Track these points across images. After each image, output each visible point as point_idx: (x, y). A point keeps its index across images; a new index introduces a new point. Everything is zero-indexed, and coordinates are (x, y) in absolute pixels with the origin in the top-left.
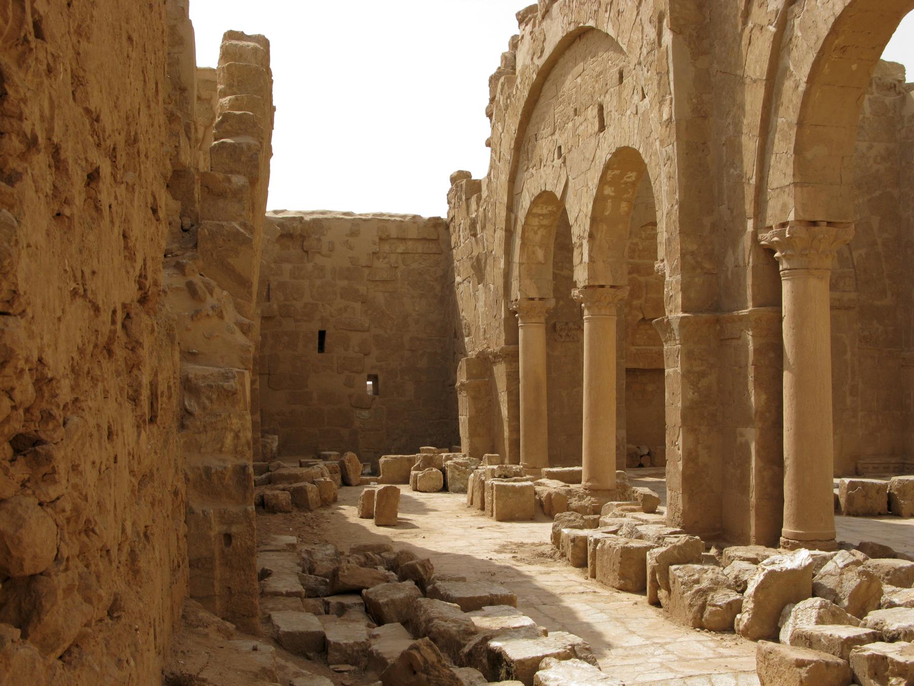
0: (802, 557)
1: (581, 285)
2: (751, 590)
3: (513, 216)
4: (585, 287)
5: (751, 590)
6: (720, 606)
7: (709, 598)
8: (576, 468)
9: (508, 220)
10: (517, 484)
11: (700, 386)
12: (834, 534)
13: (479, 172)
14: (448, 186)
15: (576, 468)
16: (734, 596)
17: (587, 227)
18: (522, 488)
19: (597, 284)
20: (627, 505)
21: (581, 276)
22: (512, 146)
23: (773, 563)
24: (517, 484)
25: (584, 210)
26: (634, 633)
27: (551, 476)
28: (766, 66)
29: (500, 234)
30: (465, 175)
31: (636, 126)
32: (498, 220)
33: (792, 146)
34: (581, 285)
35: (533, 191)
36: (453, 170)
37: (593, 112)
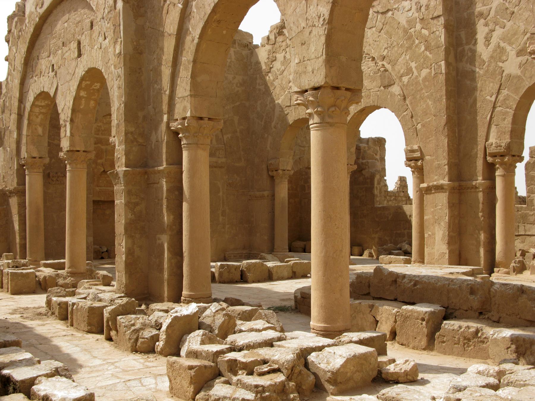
0: (192, 308)
2: (164, 328)
3: (23, 106)
4: (68, 151)
5: (164, 328)
6: (147, 338)
7: (141, 334)
8: (62, 261)
9: (19, 108)
10: (24, 271)
11: (135, 210)
15: (62, 261)
16: (155, 332)
17: (70, 115)
18: (27, 273)
19: (75, 149)
21: (65, 144)
23: (177, 312)
24: (24, 271)
25: (68, 104)
27: (46, 266)
28: (176, 27)
31: (100, 55)
33: (190, 74)
37: (74, 45)
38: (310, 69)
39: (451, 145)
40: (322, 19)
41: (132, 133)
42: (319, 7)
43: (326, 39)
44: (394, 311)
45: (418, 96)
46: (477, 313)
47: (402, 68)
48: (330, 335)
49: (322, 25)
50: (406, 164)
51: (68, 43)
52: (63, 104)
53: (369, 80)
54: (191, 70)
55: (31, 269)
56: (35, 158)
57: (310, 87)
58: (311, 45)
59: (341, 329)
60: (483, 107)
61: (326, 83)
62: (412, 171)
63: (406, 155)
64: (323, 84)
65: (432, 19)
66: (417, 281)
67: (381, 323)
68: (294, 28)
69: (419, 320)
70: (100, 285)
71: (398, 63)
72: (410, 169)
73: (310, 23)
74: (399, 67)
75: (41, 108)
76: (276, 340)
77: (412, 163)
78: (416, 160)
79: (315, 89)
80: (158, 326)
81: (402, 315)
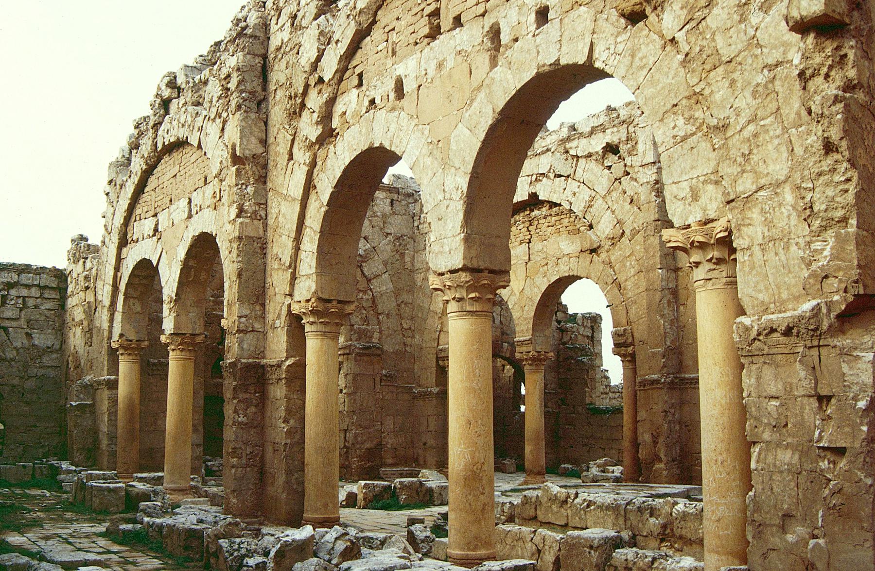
0: (307, 531)
1: (167, 332)
2: (272, 554)
3: (119, 274)
4: (171, 334)
5: (272, 554)
6: (251, 567)
7: (245, 562)
8: (160, 474)
9: (115, 277)
10: (111, 485)
11: (248, 412)
12: (339, 518)
13: (95, 239)
14: (69, 246)
15: (160, 474)
16: (260, 559)
17: (175, 290)
18: (116, 488)
19: (180, 332)
20: (105, 478)
21: (168, 325)
22: (122, 222)
23: (288, 536)
24: (111, 485)
25: (174, 276)
26: (477, 5)
27: (141, 480)
28: (301, 191)
29: (108, 289)
30: (83, 238)
31: (214, 218)
32: (107, 278)
33: (316, 247)
34: (167, 332)
35: (136, 257)
36: (75, 234)
37: (184, 203)
38: (447, 249)
39: (669, 327)
40: (460, 191)
41: (246, 316)
42: (457, 177)
43: (465, 215)
44: (558, 538)
45: (628, 264)
46: (659, 541)
47: (607, 227)
48: (469, 564)
49: (461, 198)
50: (613, 352)
51: (177, 199)
52: (168, 275)
53: (567, 242)
54: (317, 243)
55: (120, 482)
56: (131, 341)
57: (447, 270)
58: (449, 220)
59: (483, 557)
60: (152, 425)
61: (464, 265)
62: (623, 361)
63: (614, 340)
64: (460, 267)
65: (641, 166)
66: (590, 501)
67: (544, 553)
68: (431, 200)
69: (585, 549)
70: (204, 503)
71: (602, 221)
72: (620, 358)
73: (447, 196)
74: (603, 226)
75: (141, 278)
76: (399, 568)
77: (623, 350)
78: (625, 345)
79: (452, 272)
80: (266, 554)
81: (567, 542)
